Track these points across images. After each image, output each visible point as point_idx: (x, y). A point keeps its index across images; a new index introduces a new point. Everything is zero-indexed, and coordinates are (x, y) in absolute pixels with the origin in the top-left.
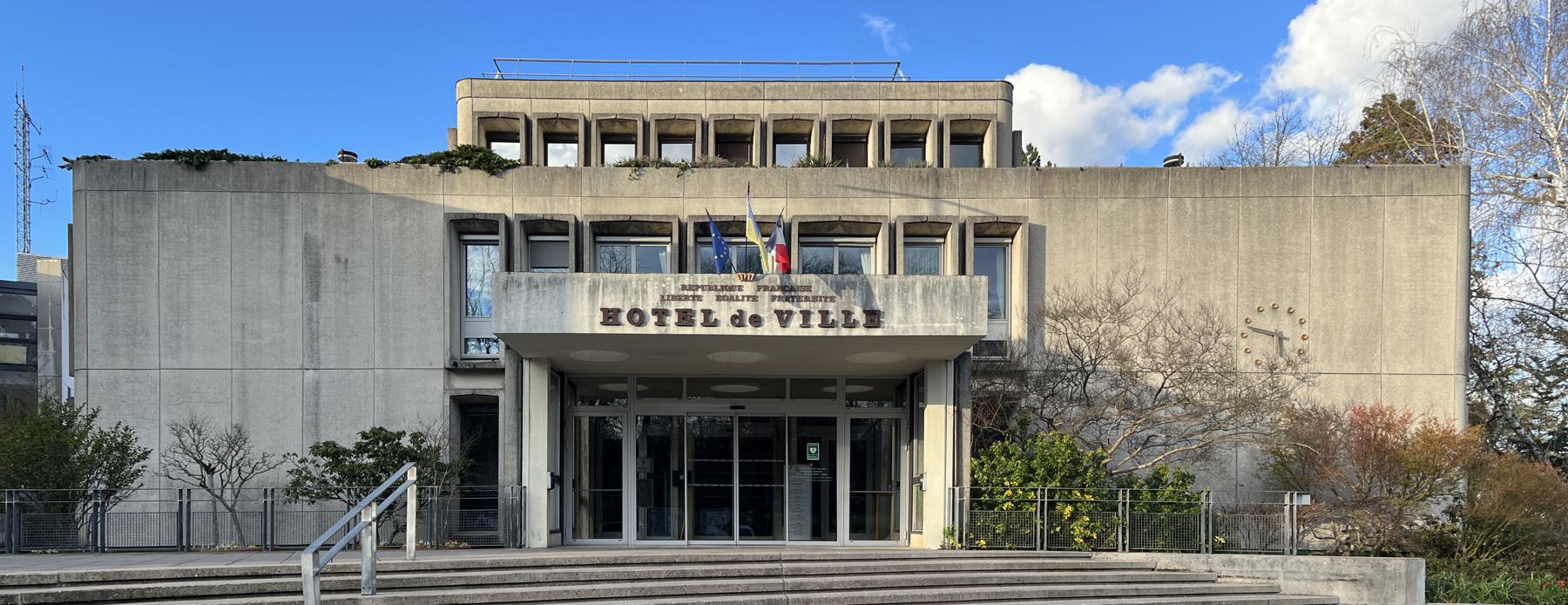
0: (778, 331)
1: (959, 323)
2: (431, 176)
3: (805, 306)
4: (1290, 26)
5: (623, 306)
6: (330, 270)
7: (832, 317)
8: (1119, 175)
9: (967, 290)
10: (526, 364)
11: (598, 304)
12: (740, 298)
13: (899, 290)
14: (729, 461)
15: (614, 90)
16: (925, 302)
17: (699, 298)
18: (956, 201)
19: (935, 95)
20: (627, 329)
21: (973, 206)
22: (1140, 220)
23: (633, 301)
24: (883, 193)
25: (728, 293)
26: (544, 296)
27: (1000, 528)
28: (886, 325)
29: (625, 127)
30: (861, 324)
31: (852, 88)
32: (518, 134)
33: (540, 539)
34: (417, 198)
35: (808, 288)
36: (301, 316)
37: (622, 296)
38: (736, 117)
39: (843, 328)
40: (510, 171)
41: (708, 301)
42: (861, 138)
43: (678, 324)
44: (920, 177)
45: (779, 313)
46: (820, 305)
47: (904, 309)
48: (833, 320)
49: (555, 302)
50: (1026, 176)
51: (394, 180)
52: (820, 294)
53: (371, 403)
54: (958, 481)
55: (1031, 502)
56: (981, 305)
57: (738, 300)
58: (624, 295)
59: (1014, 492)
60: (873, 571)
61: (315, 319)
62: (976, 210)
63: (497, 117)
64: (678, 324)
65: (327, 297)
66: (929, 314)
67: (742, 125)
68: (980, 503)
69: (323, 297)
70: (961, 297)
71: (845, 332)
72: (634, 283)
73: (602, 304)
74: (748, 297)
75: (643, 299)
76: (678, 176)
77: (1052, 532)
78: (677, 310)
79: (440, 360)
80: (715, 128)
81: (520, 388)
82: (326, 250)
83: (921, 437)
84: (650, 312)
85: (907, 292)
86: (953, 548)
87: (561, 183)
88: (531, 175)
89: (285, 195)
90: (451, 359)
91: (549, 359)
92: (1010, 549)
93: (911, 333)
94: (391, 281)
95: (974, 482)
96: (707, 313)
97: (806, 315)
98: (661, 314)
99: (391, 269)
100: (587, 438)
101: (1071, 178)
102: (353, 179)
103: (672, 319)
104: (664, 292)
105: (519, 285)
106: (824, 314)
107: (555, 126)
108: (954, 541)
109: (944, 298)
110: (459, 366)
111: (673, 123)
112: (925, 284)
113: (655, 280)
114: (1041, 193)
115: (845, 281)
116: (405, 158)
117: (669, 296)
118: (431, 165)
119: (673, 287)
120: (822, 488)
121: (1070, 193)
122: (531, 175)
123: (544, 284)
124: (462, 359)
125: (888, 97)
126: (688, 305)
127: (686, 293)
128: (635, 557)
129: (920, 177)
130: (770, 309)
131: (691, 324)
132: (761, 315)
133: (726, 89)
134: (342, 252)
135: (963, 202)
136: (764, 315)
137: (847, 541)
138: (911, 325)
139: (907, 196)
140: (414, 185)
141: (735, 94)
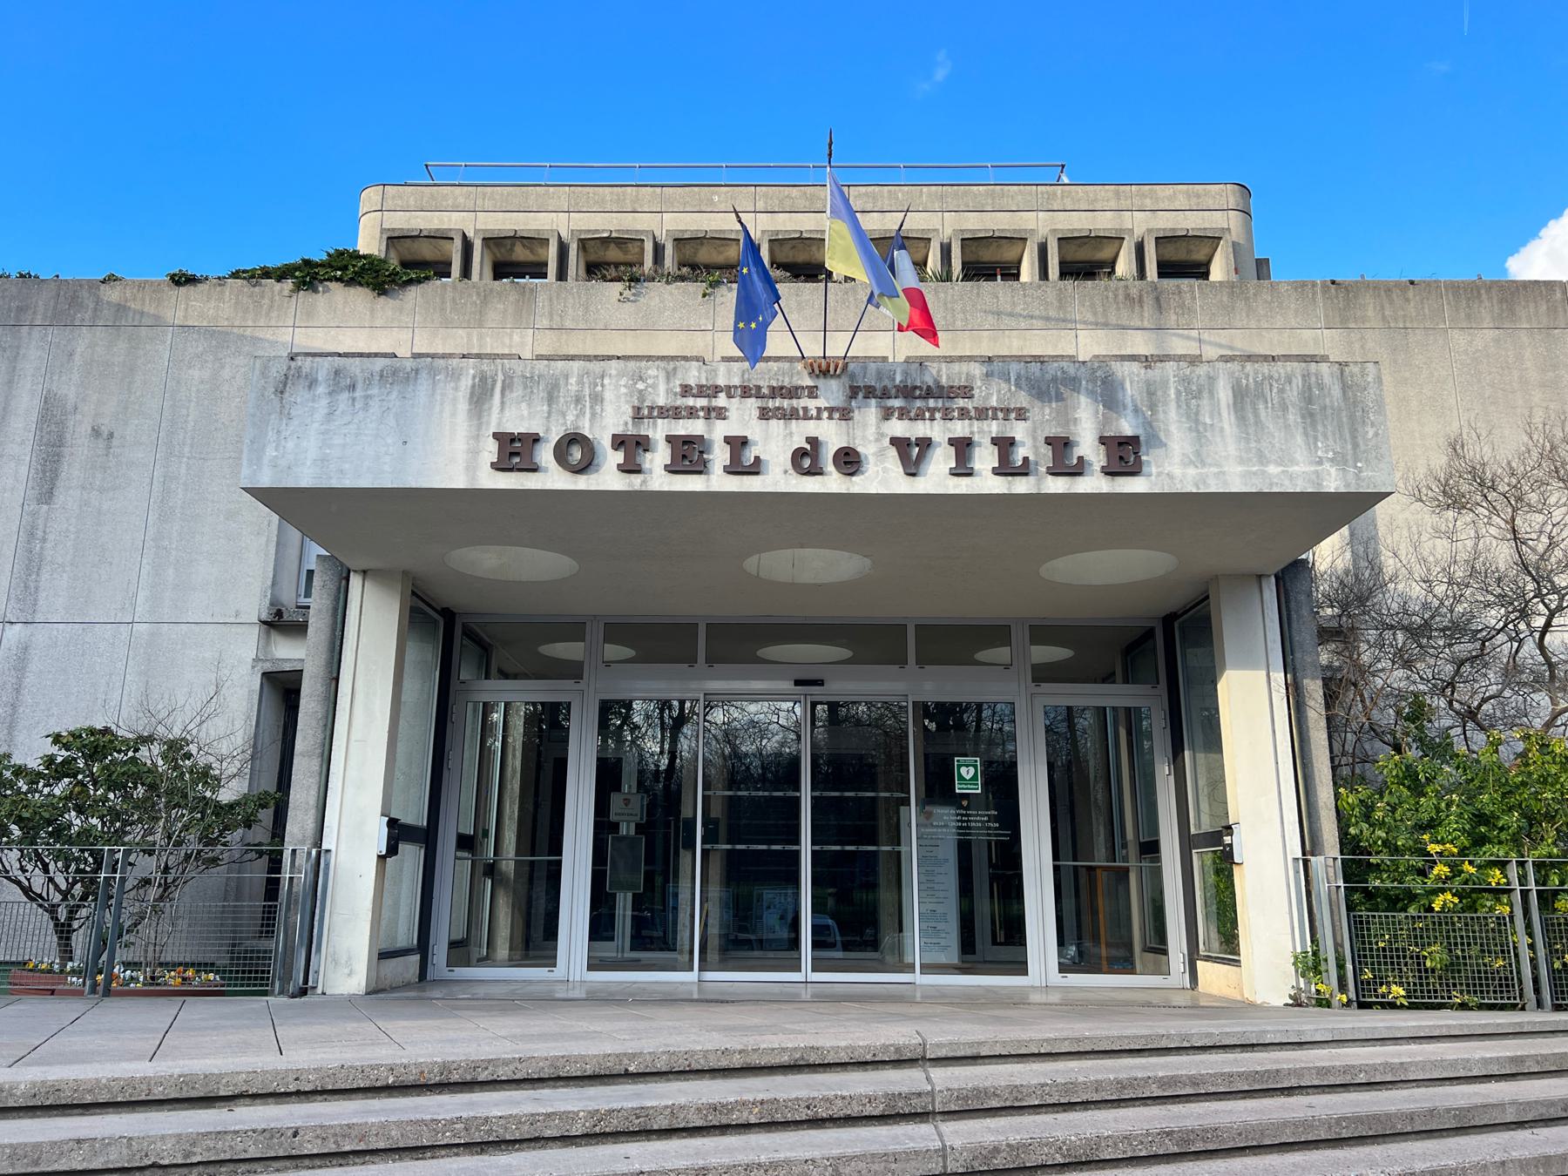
0: (899, 484)
1: (1327, 465)
2: (277, 298)
3: (960, 429)
4: (1507, 265)
5: (548, 430)
6: (80, 447)
7: (1020, 453)
8: (1479, 292)
9: (1336, 391)
10: (355, 582)
11: (488, 423)
12: (814, 413)
13: (1178, 393)
14: (790, 794)
15: (608, 198)
16: (1241, 419)
17: (721, 414)
18: (1194, 333)
19: (1125, 204)
20: (552, 478)
21: (1223, 342)
22: (1528, 364)
23: (570, 418)
24: (1064, 323)
25: (786, 403)
26: (366, 407)
27: (1435, 956)
28: (1154, 470)
29: (626, 252)
30: (1097, 467)
31: (992, 195)
32: (450, 264)
33: (350, 975)
34: (248, 332)
35: (966, 391)
36: (15, 529)
37: (545, 408)
38: (805, 235)
39: (1050, 477)
40: (413, 288)
41: (741, 418)
42: (1009, 268)
43: (672, 469)
44: (1127, 296)
45: (900, 444)
46: (994, 428)
47: (1194, 434)
48: (1026, 459)
49: (391, 421)
50: (1314, 293)
51: (213, 304)
52: (994, 404)
53: (119, 684)
54: (1311, 845)
55: (1498, 893)
56: (1373, 425)
57: (807, 417)
58: (549, 405)
59: (1456, 870)
60: (1189, 1091)
61: (40, 534)
62: (1231, 348)
63: (418, 236)
64: (672, 469)
65: (68, 496)
66: (1253, 445)
67: (814, 248)
68: (1369, 895)
69: (60, 497)
70: (1324, 408)
71: (1057, 485)
72: (573, 380)
73: (499, 424)
74: (831, 410)
75: (593, 415)
76: (704, 296)
77: (1557, 965)
78: (670, 439)
79: (255, 607)
80: (771, 252)
81: (338, 633)
82: (79, 417)
83: (1213, 741)
84: (606, 442)
85: (1198, 396)
86: (1323, 1002)
87: (500, 306)
88: (449, 294)
89: (25, 330)
90: (272, 604)
91: (405, 573)
92: (1463, 1006)
93: (1213, 488)
94: (183, 471)
95: (1348, 843)
96: (738, 444)
97: (963, 447)
98: (632, 446)
99: (187, 449)
100: (519, 754)
101: (1394, 296)
102: (143, 304)
103: (659, 457)
104: (642, 398)
105: (312, 384)
106: (1005, 445)
107: (512, 250)
108: (1328, 987)
109: (1284, 408)
110: (285, 617)
111: (702, 244)
112: (1238, 381)
113: (621, 375)
114: (1344, 320)
115: (1048, 377)
116: (238, 272)
117: (651, 408)
118: (278, 281)
119: (662, 388)
120: (974, 851)
121: (1396, 320)
122: (449, 294)
123: (368, 382)
124: (298, 607)
125: (1050, 208)
126: (695, 427)
127: (690, 402)
128: (506, 1063)
129: (1127, 296)
130: (881, 435)
131: (700, 468)
132: (859, 449)
133: (787, 197)
134: (106, 422)
135: (1206, 336)
136: (866, 449)
137: (1056, 978)
138: (1215, 470)
139: (1106, 325)
140: (246, 311)
141: (801, 204)
